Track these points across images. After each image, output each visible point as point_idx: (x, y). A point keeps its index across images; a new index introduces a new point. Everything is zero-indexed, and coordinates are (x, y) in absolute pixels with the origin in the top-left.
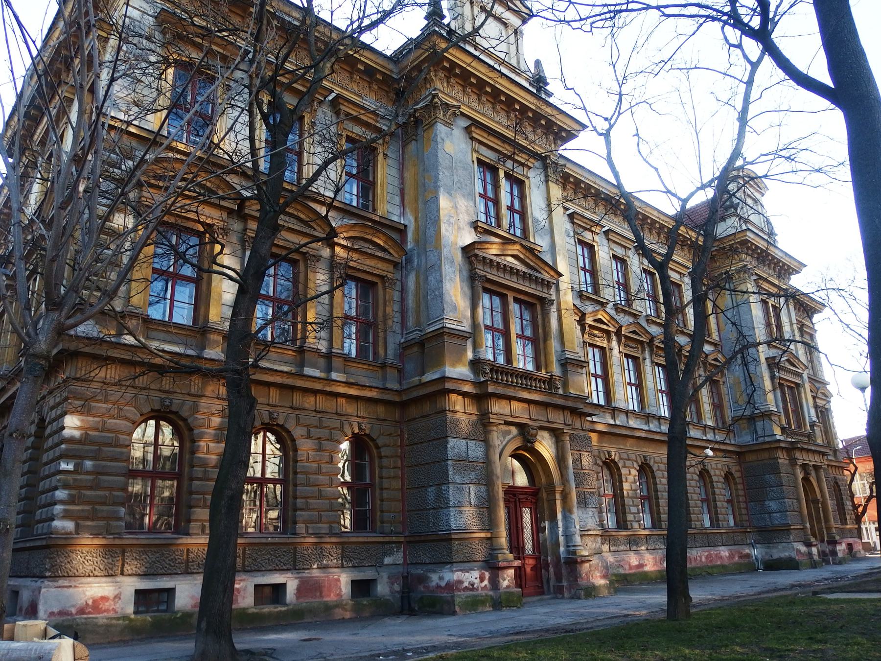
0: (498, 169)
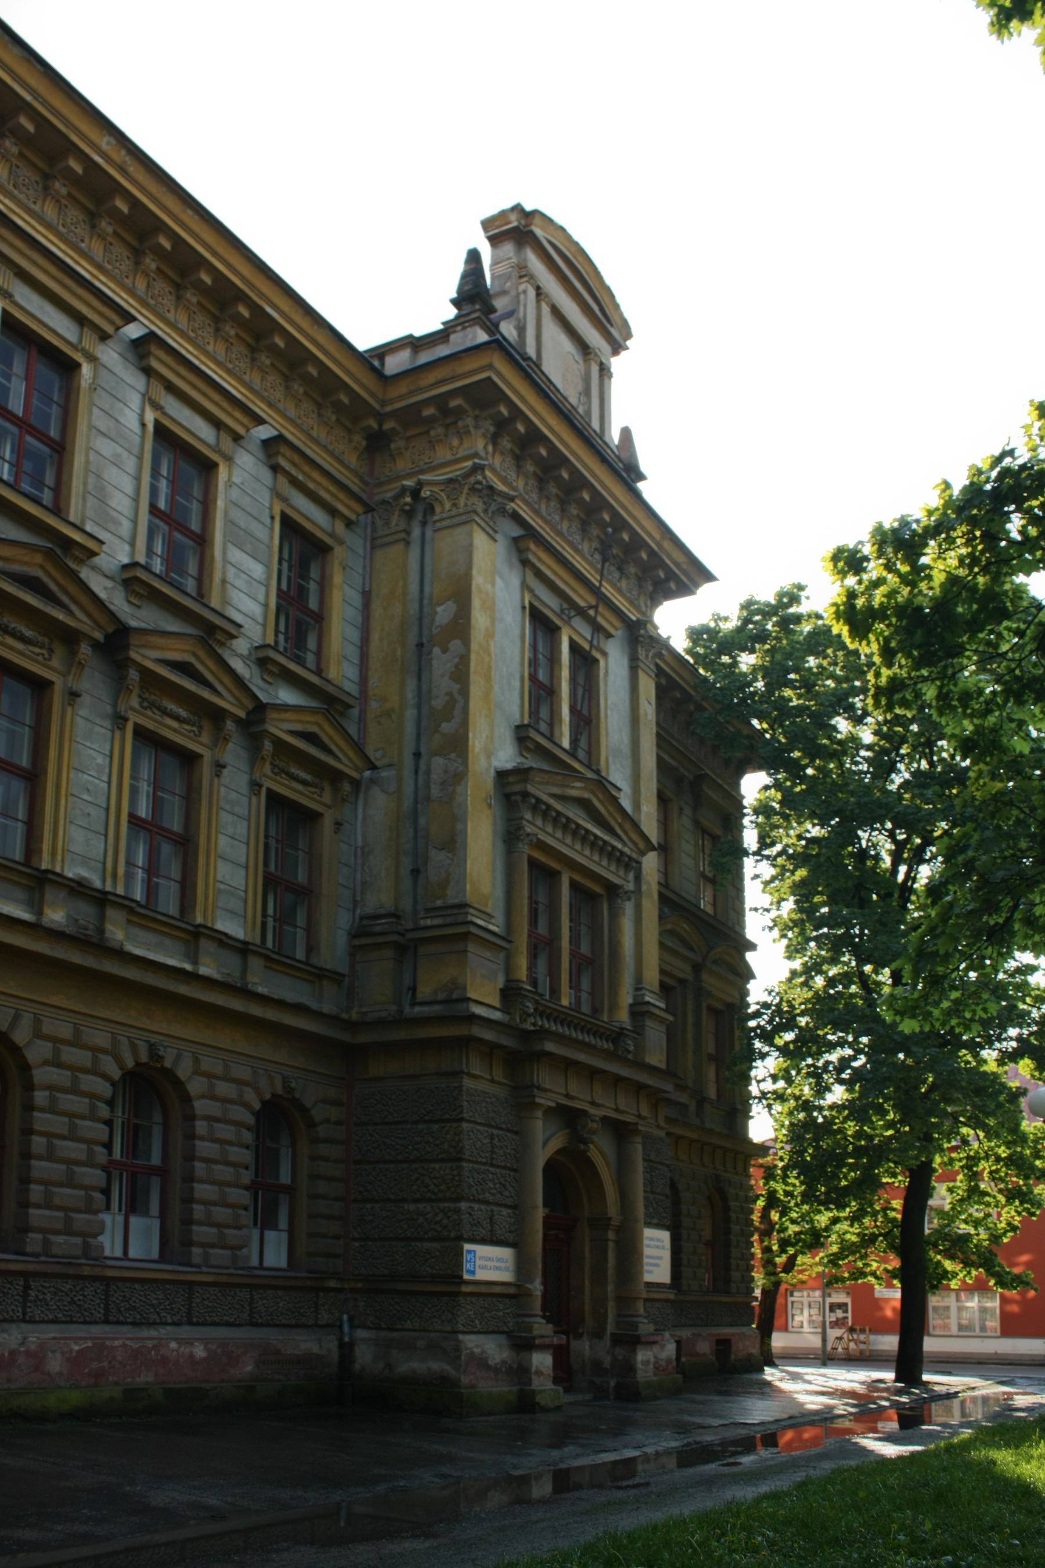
0: (558, 629)
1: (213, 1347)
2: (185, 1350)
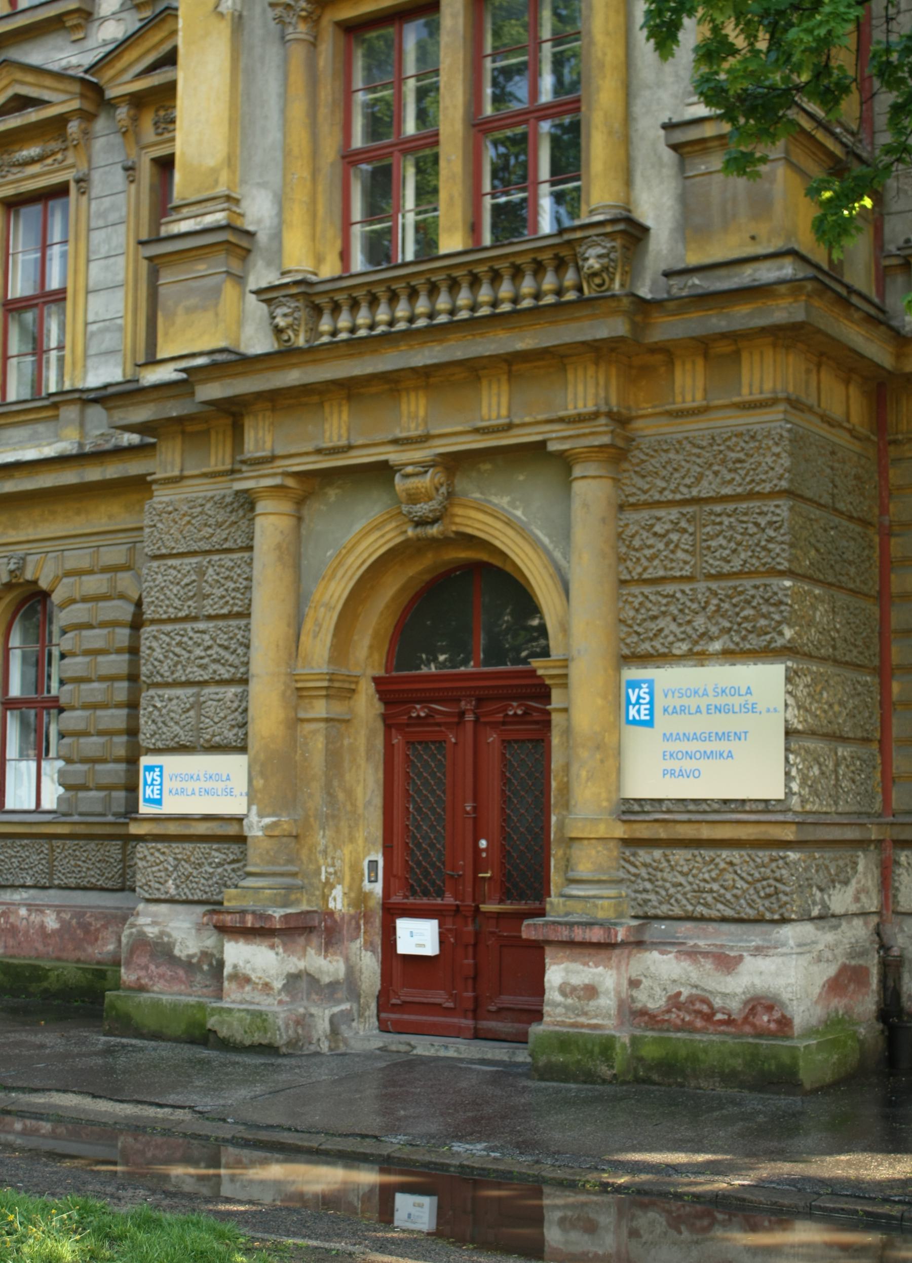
1: (66, 916)
2: (35, 918)
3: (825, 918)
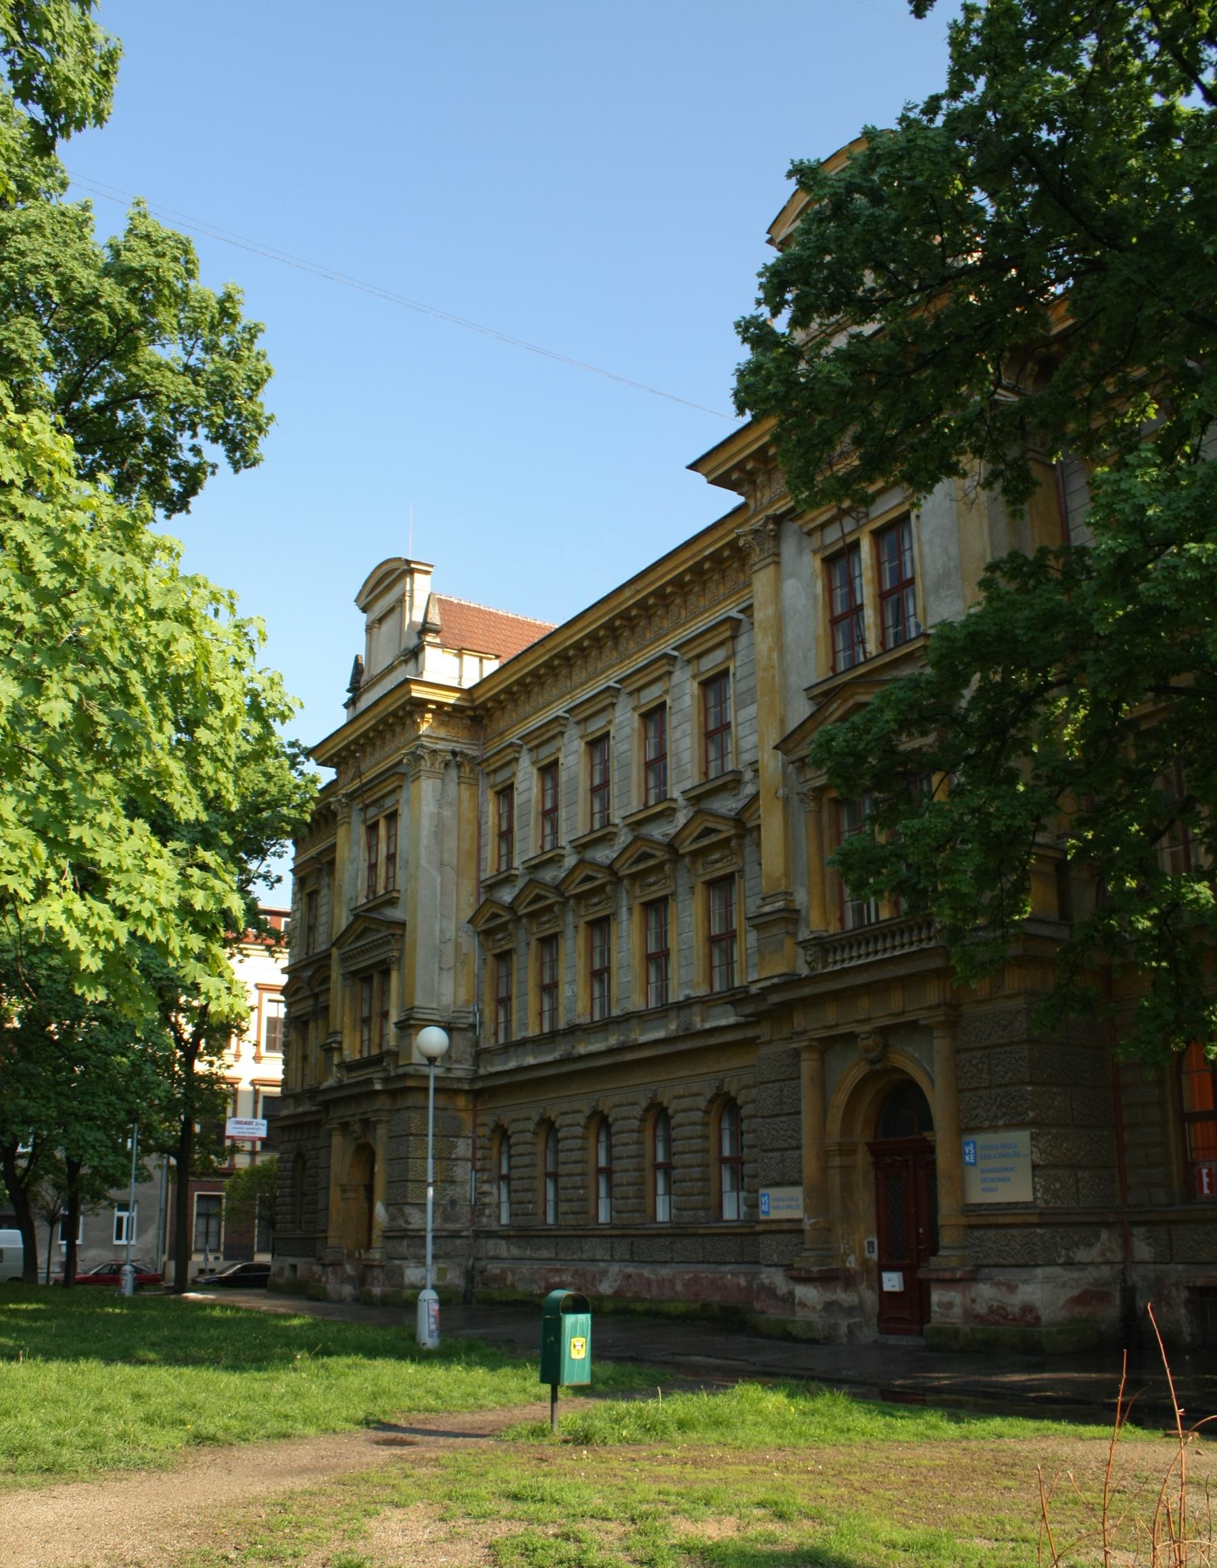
2: (735, 1280)
3: (1070, 1264)
